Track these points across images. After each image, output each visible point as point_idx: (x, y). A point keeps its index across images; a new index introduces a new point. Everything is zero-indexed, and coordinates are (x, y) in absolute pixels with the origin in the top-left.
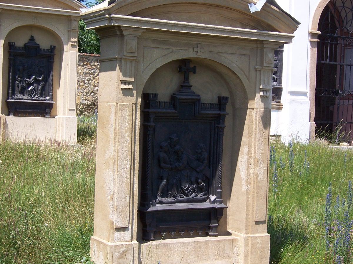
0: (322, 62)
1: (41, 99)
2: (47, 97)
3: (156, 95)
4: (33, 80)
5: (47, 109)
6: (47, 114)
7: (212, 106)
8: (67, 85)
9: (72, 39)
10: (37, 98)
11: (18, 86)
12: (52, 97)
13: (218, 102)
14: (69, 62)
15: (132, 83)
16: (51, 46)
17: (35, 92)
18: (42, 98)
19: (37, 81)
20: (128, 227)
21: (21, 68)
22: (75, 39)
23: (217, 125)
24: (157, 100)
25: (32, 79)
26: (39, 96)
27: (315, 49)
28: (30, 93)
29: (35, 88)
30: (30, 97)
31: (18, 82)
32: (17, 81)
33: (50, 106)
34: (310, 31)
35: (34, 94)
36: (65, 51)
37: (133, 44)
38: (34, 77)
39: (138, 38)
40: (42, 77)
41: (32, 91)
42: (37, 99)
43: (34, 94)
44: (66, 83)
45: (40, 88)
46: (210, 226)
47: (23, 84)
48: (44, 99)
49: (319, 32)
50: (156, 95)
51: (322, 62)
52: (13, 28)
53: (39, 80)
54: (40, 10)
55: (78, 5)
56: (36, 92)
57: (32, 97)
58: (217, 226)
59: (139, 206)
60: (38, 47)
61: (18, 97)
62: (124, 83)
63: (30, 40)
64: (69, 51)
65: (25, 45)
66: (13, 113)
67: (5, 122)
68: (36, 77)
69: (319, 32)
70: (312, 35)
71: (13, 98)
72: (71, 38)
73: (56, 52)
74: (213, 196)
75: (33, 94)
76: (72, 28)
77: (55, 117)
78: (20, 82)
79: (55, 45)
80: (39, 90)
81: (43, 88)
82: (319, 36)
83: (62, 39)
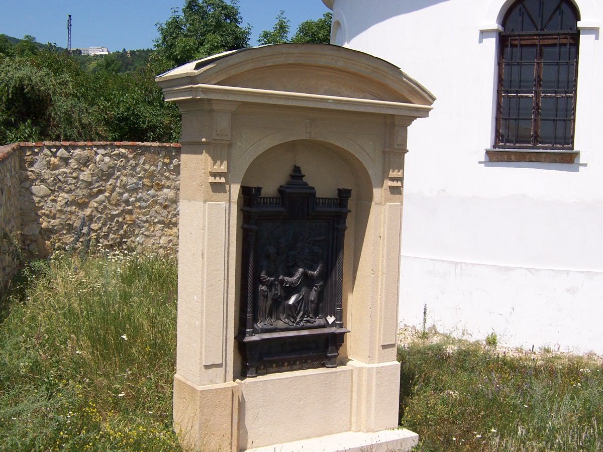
1: (316, 323)
2: (329, 317)
3: (259, 190)
4: (299, 278)
5: (330, 348)
6: (329, 358)
7: (327, 201)
8: (379, 287)
9: (393, 171)
10: (308, 321)
11: (266, 297)
12: (340, 317)
13: (339, 196)
14: (384, 231)
15: (224, 175)
16: (340, 191)
17: (302, 308)
18: (319, 321)
19: (308, 280)
20: (222, 364)
21: (272, 250)
22: (399, 172)
23: (336, 226)
24: (260, 195)
25: (298, 275)
26: (311, 318)
28: (292, 312)
29: (302, 298)
30: (293, 322)
31: (264, 288)
32: (263, 285)
33: (337, 340)
35: (302, 313)
36: (376, 204)
37: (223, 123)
38: (301, 270)
39: (233, 114)
40: (319, 268)
41: (296, 308)
42: (309, 324)
43: (302, 313)
44: (378, 281)
45: (313, 296)
46: (328, 356)
47: (276, 292)
48: (322, 322)
50: (259, 190)
52: (261, 150)
53: (312, 276)
54: (330, 103)
55: (413, 89)
56: (305, 308)
57: (298, 320)
58: (336, 356)
59: (237, 332)
60: (310, 194)
61: (265, 327)
62: (219, 175)
63: (292, 177)
64: (385, 204)
65: (281, 191)
66: (254, 369)
67: (240, 398)
68: (306, 270)
71: (255, 332)
72: (391, 170)
73: (351, 203)
74: (331, 317)
75: (298, 315)
76: (396, 147)
77: (346, 365)
78: (270, 286)
79: (350, 188)
80: (312, 302)
81: (320, 295)
83: (370, 172)
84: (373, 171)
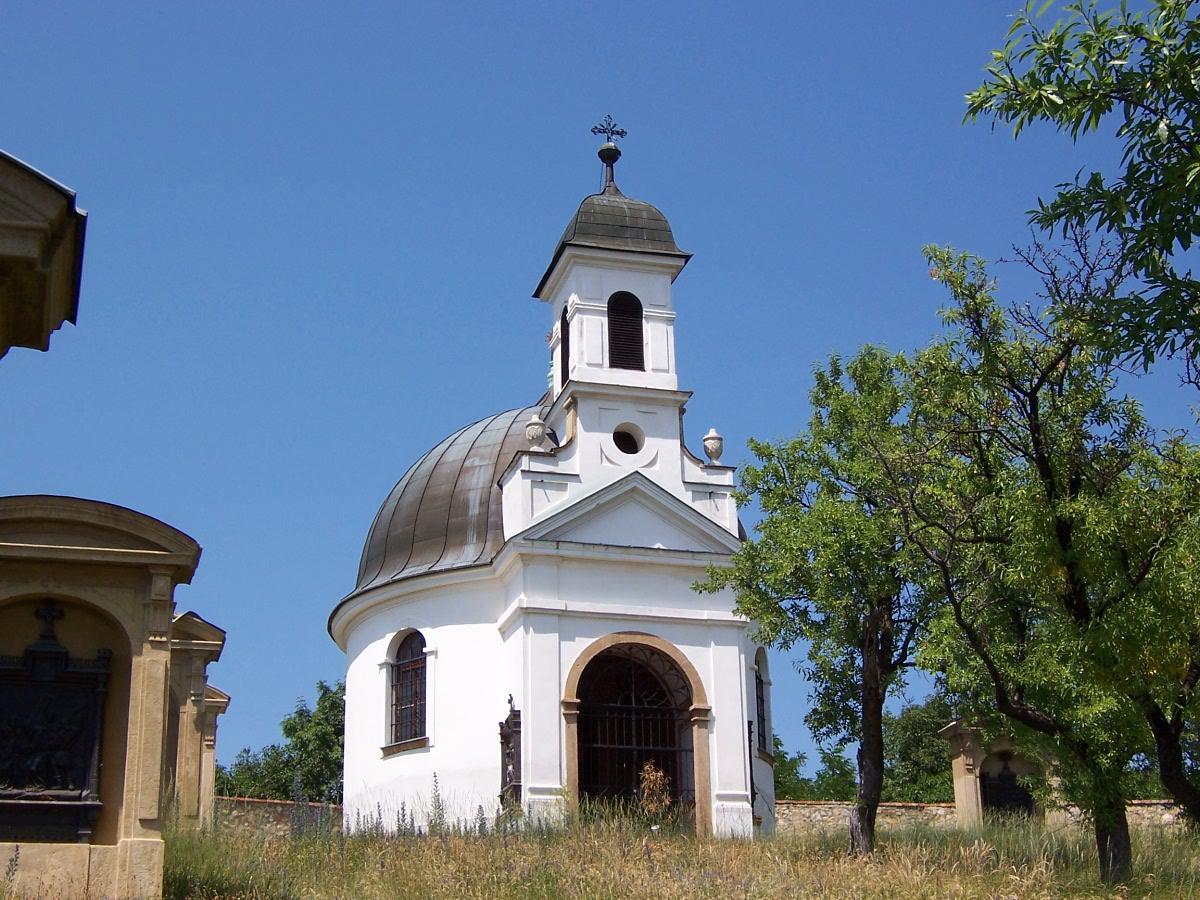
0: (595, 745)
27: (574, 726)
34: (563, 698)
49: (579, 701)
51: (595, 745)
69: (579, 701)
70: (566, 705)
76: (154, 597)
82: (578, 707)
84: (129, 627)
